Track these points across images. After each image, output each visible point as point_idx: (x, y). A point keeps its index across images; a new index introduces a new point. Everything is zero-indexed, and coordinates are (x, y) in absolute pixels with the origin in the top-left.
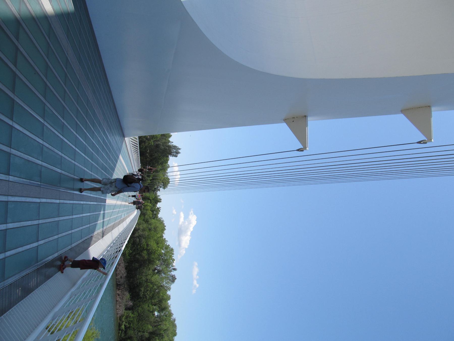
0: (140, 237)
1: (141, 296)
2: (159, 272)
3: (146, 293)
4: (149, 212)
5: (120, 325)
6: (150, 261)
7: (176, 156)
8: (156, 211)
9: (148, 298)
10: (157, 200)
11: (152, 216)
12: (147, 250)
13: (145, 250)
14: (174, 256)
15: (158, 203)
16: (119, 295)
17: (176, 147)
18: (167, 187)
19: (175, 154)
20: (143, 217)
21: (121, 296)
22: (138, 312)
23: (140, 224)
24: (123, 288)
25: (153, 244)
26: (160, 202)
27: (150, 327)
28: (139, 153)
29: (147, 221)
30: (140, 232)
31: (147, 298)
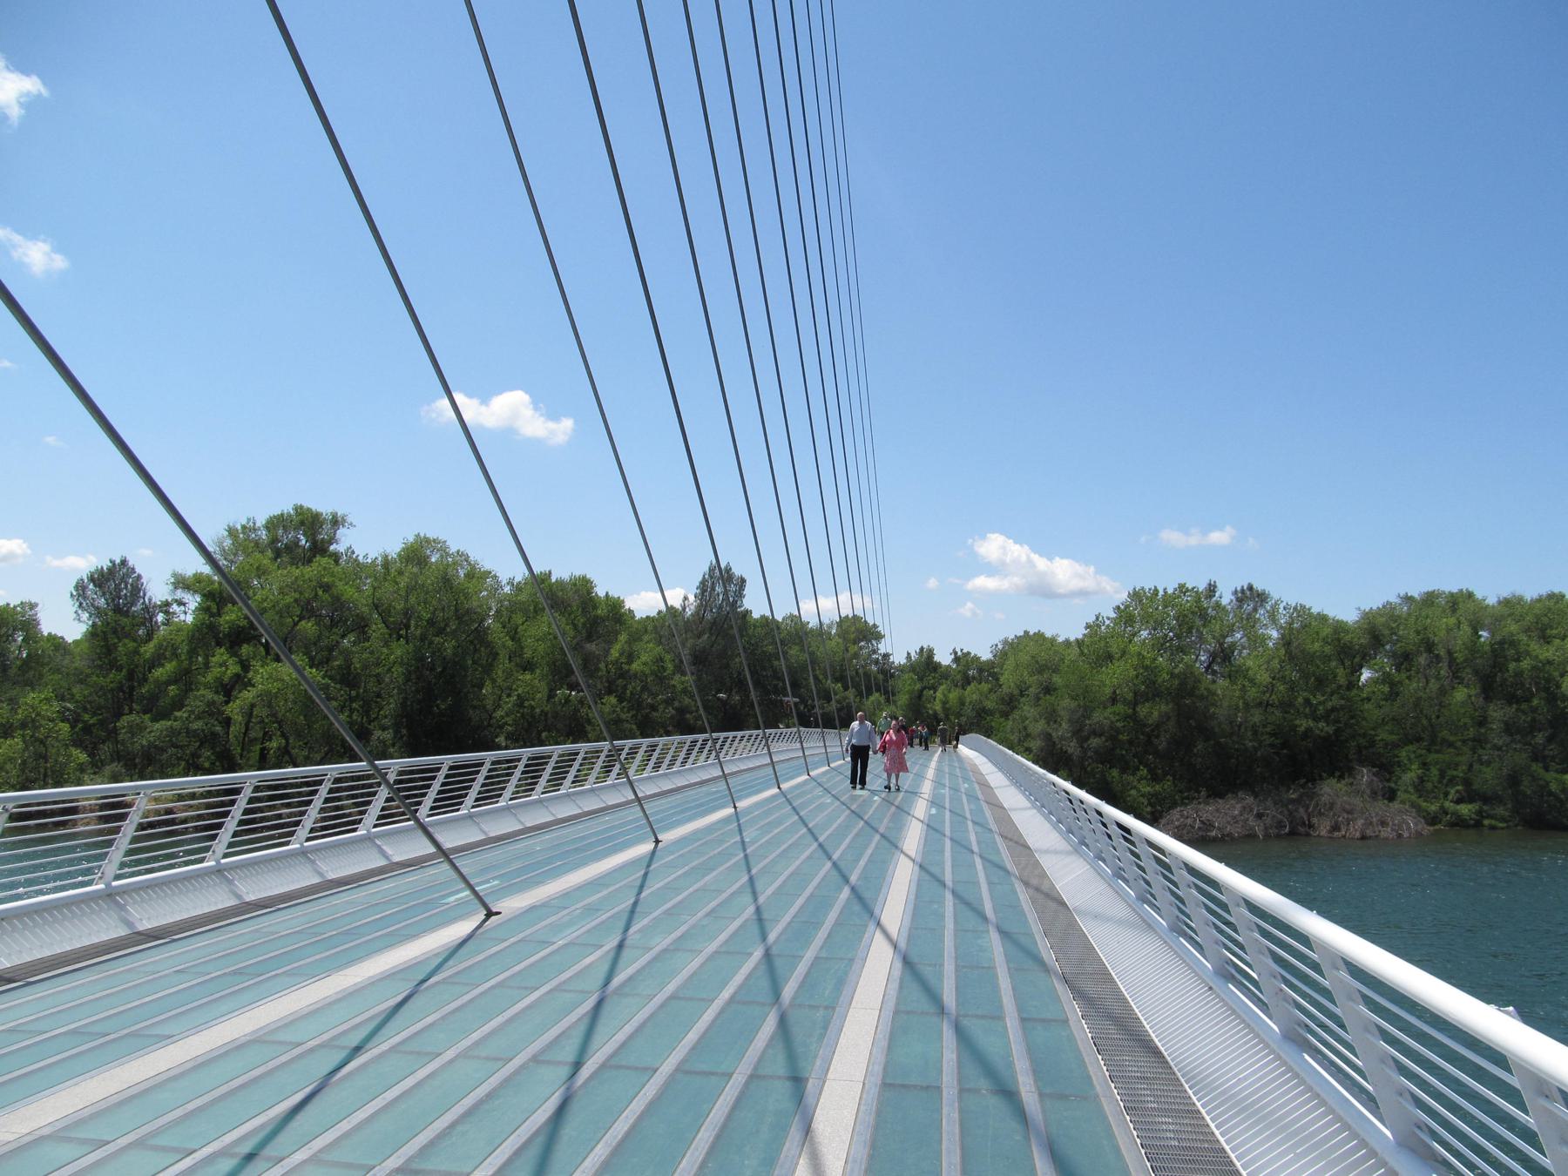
0: (1080, 730)
1: (1330, 729)
2: (1223, 655)
3: (1321, 708)
4: (972, 693)
5: (1459, 823)
6: (1185, 691)
7: (743, 581)
8: (968, 667)
9: (1343, 702)
10: (925, 664)
11: (987, 681)
12: (1134, 704)
13: (1134, 709)
14: (1165, 589)
15: (937, 658)
16: (1336, 828)
17: (703, 582)
18: (874, 624)
19: (733, 588)
20: (996, 721)
21: (1340, 819)
22: (1396, 746)
23: (1025, 728)
24: (1301, 810)
25: (1115, 676)
26: (931, 653)
27: (1460, 694)
28: (731, 734)
29: (1010, 704)
30: (1063, 729)
31: (1341, 705)
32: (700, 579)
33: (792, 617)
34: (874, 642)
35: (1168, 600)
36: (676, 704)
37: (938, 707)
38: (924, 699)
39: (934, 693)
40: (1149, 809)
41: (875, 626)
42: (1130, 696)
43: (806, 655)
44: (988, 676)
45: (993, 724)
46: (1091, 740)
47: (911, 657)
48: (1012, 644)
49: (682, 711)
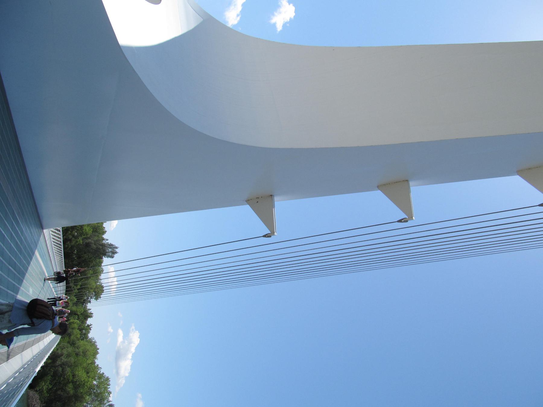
0: (64, 365)
4: (77, 332)
7: (113, 257)
10: (87, 315)
12: (73, 382)
15: (89, 319)
17: (112, 245)
23: (64, 348)
25: (81, 374)
30: (64, 359)
32: (113, 244)
33: (103, 271)
34: (95, 297)
35: (106, 388)
36: (73, 239)
37: (71, 321)
38: (74, 316)
39: (77, 319)
40: (38, 389)
41: (100, 297)
42: (75, 380)
43: (89, 276)
44: (83, 337)
45: (66, 338)
46: (61, 368)
47: (89, 310)
48: (94, 344)
49: (70, 240)
